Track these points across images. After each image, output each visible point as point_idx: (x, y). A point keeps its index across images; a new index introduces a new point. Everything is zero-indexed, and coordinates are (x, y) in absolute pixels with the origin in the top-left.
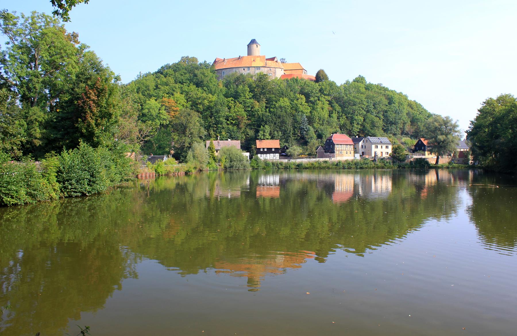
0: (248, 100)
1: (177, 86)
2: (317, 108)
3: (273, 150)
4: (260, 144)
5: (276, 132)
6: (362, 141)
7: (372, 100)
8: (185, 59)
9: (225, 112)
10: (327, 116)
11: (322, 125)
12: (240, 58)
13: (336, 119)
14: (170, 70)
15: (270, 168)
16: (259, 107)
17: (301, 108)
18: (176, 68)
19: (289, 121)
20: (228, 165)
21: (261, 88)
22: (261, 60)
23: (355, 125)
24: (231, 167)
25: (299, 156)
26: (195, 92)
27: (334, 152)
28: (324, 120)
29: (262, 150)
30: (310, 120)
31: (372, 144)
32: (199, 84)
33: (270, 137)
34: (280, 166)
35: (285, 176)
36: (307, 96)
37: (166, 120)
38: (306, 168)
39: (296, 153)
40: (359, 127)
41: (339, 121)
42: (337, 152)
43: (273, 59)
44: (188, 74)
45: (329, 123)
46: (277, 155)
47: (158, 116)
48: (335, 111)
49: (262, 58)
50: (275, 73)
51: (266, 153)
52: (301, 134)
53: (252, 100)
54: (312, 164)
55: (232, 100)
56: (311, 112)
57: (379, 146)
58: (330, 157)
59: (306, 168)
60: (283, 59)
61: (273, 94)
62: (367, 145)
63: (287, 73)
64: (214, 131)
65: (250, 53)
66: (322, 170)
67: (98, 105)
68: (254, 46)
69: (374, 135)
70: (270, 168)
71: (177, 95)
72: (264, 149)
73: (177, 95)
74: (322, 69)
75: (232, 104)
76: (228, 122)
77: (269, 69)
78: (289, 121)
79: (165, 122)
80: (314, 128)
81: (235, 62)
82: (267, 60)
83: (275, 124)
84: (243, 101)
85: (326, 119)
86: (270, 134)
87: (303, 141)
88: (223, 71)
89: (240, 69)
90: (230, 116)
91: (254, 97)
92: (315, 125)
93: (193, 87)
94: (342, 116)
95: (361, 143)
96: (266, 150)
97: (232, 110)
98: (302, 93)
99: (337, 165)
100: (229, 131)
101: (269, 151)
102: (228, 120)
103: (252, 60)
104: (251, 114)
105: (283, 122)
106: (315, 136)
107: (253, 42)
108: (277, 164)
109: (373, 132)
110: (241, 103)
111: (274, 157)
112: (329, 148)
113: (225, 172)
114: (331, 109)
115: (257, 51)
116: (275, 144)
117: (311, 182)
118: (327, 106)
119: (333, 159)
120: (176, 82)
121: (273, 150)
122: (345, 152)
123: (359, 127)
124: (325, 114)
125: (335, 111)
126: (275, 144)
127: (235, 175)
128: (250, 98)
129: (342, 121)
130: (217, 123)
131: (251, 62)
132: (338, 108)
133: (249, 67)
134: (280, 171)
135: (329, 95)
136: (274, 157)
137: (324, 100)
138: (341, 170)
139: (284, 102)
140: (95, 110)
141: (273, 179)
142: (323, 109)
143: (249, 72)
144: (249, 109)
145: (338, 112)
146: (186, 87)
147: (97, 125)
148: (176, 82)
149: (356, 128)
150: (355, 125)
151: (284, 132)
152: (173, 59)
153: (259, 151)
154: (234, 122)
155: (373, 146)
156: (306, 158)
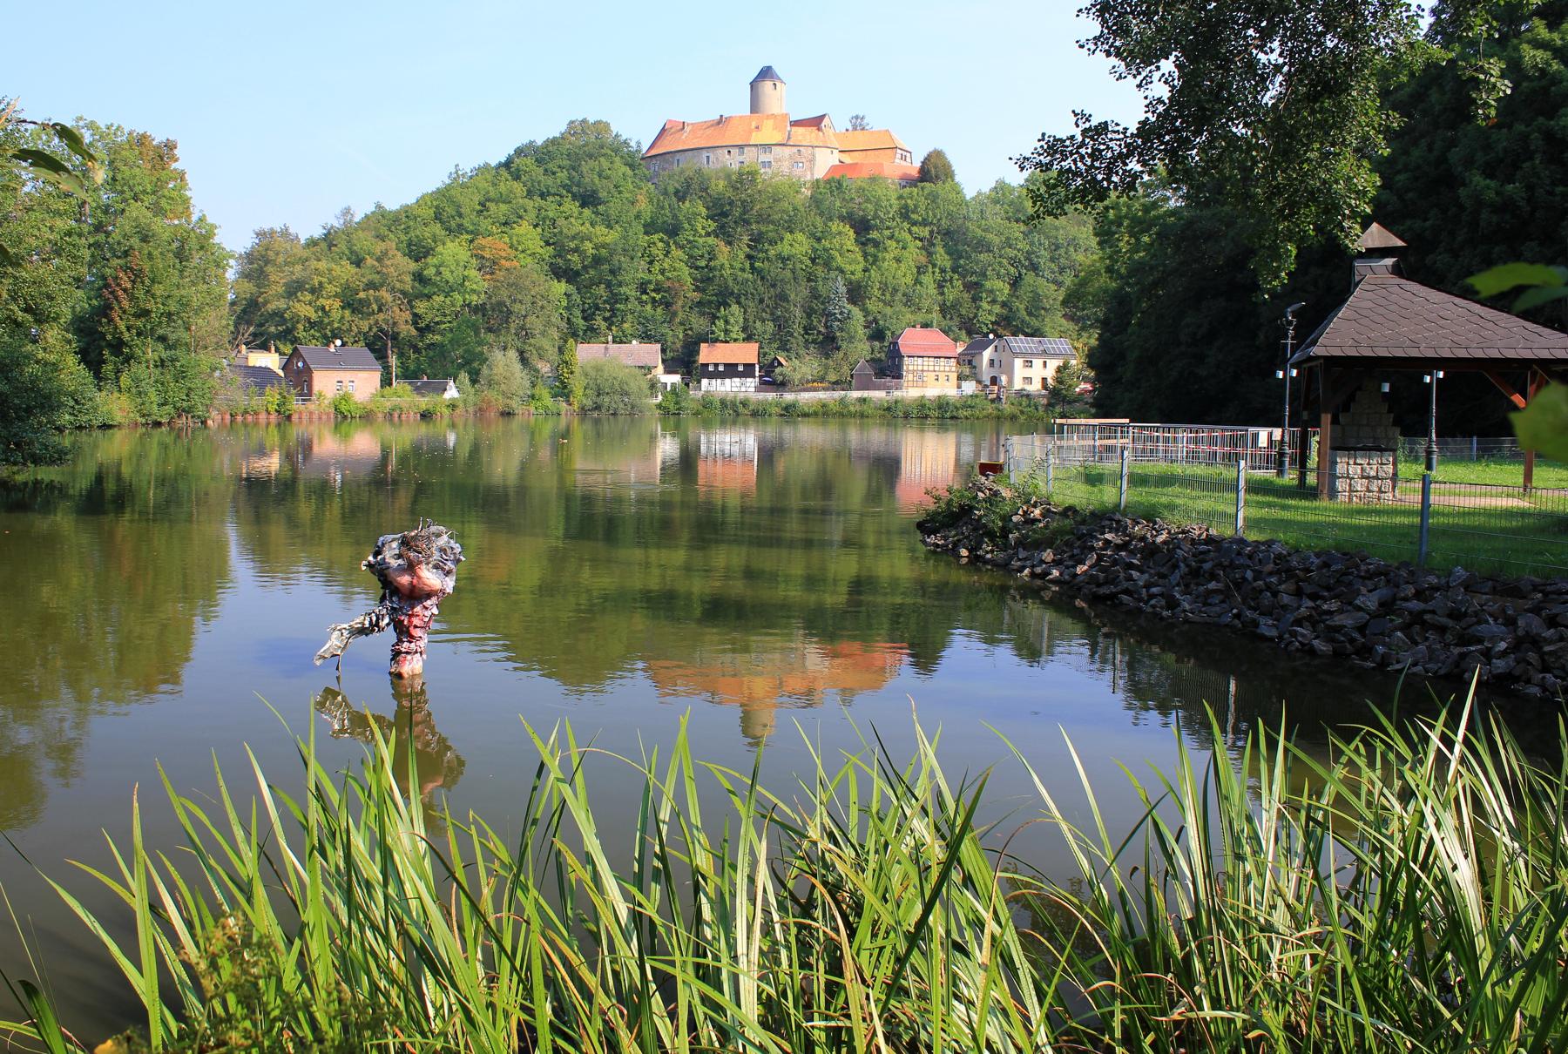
0: (701, 240)
1: (529, 204)
2: (884, 259)
3: (741, 368)
4: (708, 354)
5: (758, 324)
6: (991, 348)
7: (1048, 237)
8: (579, 129)
9: (637, 271)
10: (909, 280)
11: (890, 304)
12: (721, 121)
13: (932, 290)
14: (529, 161)
15: (734, 413)
16: (729, 258)
17: (608, 240)
18: (542, 154)
19: (798, 294)
20: (589, 403)
21: (739, 209)
22: (775, 128)
23: (985, 305)
24: (598, 408)
25: (804, 386)
26: (576, 221)
27: (900, 376)
28: (895, 290)
29: (711, 369)
30: (856, 294)
31: (1016, 355)
32: (588, 199)
33: (743, 335)
34: (741, 409)
35: (770, 432)
36: (862, 227)
37: (479, 294)
38: (806, 415)
39: (797, 377)
40: (997, 309)
41: (942, 294)
42: (908, 377)
43: (816, 122)
44: (569, 170)
45: (909, 301)
46: (751, 384)
47: (461, 286)
48: (934, 266)
49: (779, 119)
50: (812, 161)
51: (722, 376)
52: (826, 327)
53: (711, 240)
54: (824, 406)
55: (661, 240)
56: (865, 270)
57: (1037, 362)
58: (888, 389)
59: (806, 415)
60: (857, 117)
61: (772, 222)
62: (1005, 357)
63: (847, 159)
64: (605, 319)
65: (755, 106)
66: (831, 420)
67: (132, 298)
68: (767, 85)
69: (1036, 333)
70: (734, 413)
71: (524, 229)
72: (716, 365)
73: (524, 229)
74: (939, 147)
75: (658, 250)
76: (644, 297)
77: (795, 150)
78: (798, 294)
79: (475, 297)
80: (866, 312)
81: (709, 132)
82: (796, 123)
83: (761, 301)
84: (689, 242)
85: (902, 289)
86: (744, 329)
87: (828, 344)
88: (678, 156)
89: (720, 151)
90: (650, 282)
91: (723, 232)
92: (870, 306)
93: (571, 206)
94: (951, 280)
95: (987, 354)
96: (721, 368)
97: (657, 267)
98: (849, 219)
99: (888, 409)
100: (643, 321)
101: (731, 371)
102: (644, 292)
103: (754, 125)
104: (705, 278)
105: (783, 297)
106: (861, 332)
107: (766, 73)
108: (733, 404)
109: (1035, 323)
110: (682, 247)
111: (744, 388)
112: (889, 367)
113: (583, 420)
114: (923, 260)
115: (779, 100)
116: (746, 353)
117: (842, 453)
118: (914, 254)
119: (897, 394)
120: (530, 194)
121: (741, 368)
122: (931, 375)
123: (997, 309)
124: (903, 275)
125: (934, 266)
126: (746, 353)
127: (606, 427)
128: (708, 234)
129: (951, 294)
130: (615, 299)
131: (750, 132)
132: (942, 257)
133: (741, 147)
134: (741, 419)
135: (924, 223)
136: (744, 388)
137: (908, 238)
138: (949, 422)
139: (797, 245)
140: (126, 304)
141: (740, 443)
142: (901, 260)
143: (741, 158)
144: (703, 263)
145: (943, 271)
146: (554, 206)
147: (129, 328)
148: (530, 194)
149: (988, 313)
150: (985, 305)
151: (781, 325)
152: (545, 128)
153: (707, 372)
154: (658, 297)
155: (1018, 362)
156: (824, 389)
